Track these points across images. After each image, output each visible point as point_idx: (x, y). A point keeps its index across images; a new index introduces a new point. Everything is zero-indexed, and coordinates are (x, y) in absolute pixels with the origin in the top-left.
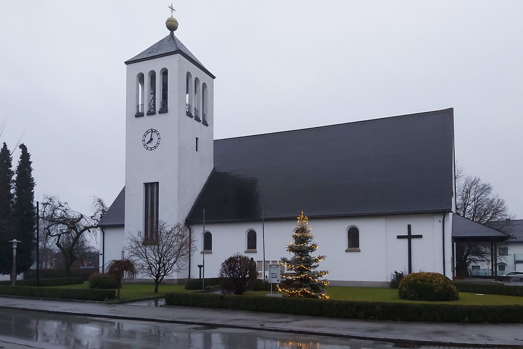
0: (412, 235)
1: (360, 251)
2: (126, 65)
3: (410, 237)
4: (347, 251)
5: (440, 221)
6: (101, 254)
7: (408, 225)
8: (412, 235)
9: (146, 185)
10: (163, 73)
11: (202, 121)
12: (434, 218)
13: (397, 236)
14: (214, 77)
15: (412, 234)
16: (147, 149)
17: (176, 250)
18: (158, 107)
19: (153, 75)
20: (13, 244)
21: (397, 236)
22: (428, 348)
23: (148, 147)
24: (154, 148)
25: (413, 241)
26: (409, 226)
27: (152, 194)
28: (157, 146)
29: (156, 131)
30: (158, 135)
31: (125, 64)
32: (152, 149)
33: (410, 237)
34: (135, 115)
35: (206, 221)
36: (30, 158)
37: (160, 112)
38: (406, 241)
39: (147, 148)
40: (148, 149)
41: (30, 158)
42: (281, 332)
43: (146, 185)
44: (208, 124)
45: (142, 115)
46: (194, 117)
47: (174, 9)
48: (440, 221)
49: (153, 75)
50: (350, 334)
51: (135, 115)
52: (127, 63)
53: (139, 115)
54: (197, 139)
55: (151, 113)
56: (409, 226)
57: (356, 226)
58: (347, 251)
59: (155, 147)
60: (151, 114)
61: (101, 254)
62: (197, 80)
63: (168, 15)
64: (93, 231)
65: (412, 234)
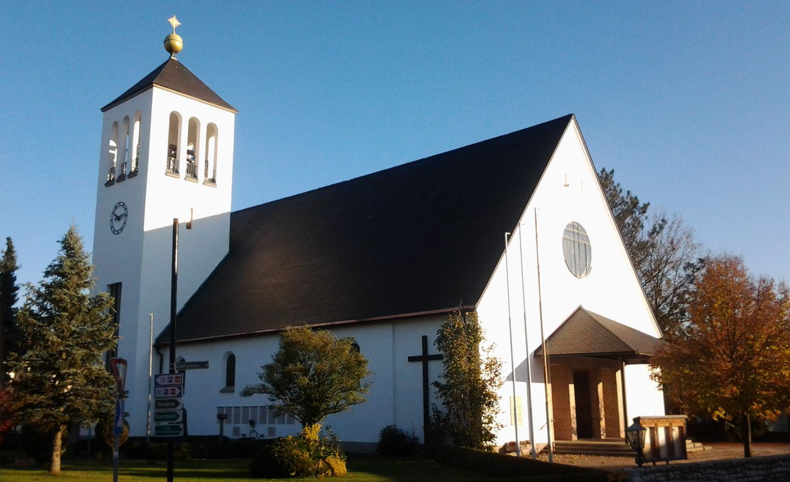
4: (222, 391)
7: (423, 337)
31: (102, 111)
38: (419, 365)
52: (104, 109)
58: (222, 391)
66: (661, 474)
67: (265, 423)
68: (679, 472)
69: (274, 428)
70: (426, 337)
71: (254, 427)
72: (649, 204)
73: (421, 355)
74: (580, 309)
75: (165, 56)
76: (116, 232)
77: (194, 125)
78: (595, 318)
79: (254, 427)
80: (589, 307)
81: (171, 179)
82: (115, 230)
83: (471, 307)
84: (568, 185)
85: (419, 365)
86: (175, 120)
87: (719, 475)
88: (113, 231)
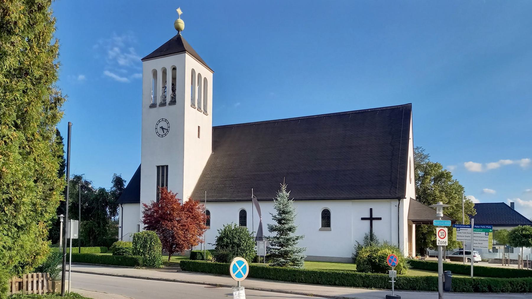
0: (373, 217)
1: (331, 231)
3: (371, 219)
4: (320, 230)
5: (396, 206)
6: (120, 227)
7: (370, 209)
8: (373, 217)
9: (158, 167)
10: (173, 69)
11: (203, 112)
12: (391, 203)
15: (373, 217)
16: (159, 136)
17: (41, 160)
18: (168, 99)
19: (164, 72)
20: (61, 219)
21: (361, 218)
22: (229, 226)
23: (160, 135)
24: (165, 135)
26: (371, 210)
27: (163, 175)
28: (167, 133)
32: (163, 136)
33: (371, 219)
37: (170, 104)
38: (368, 222)
40: (160, 136)
42: (76, 272)
43: (158, 167)
46: (197, 108)
48: (396, 206)
49: (164, 72)
55: (163, 104)
56: (371, 210)
57: (330, 209)
58: (320, 230)
60: (162, 105)
61: (120, 227)
62: (199, 75)
64: (283, 273)
65: (373, 217)
70: (372, 209)
86: (193, 71)
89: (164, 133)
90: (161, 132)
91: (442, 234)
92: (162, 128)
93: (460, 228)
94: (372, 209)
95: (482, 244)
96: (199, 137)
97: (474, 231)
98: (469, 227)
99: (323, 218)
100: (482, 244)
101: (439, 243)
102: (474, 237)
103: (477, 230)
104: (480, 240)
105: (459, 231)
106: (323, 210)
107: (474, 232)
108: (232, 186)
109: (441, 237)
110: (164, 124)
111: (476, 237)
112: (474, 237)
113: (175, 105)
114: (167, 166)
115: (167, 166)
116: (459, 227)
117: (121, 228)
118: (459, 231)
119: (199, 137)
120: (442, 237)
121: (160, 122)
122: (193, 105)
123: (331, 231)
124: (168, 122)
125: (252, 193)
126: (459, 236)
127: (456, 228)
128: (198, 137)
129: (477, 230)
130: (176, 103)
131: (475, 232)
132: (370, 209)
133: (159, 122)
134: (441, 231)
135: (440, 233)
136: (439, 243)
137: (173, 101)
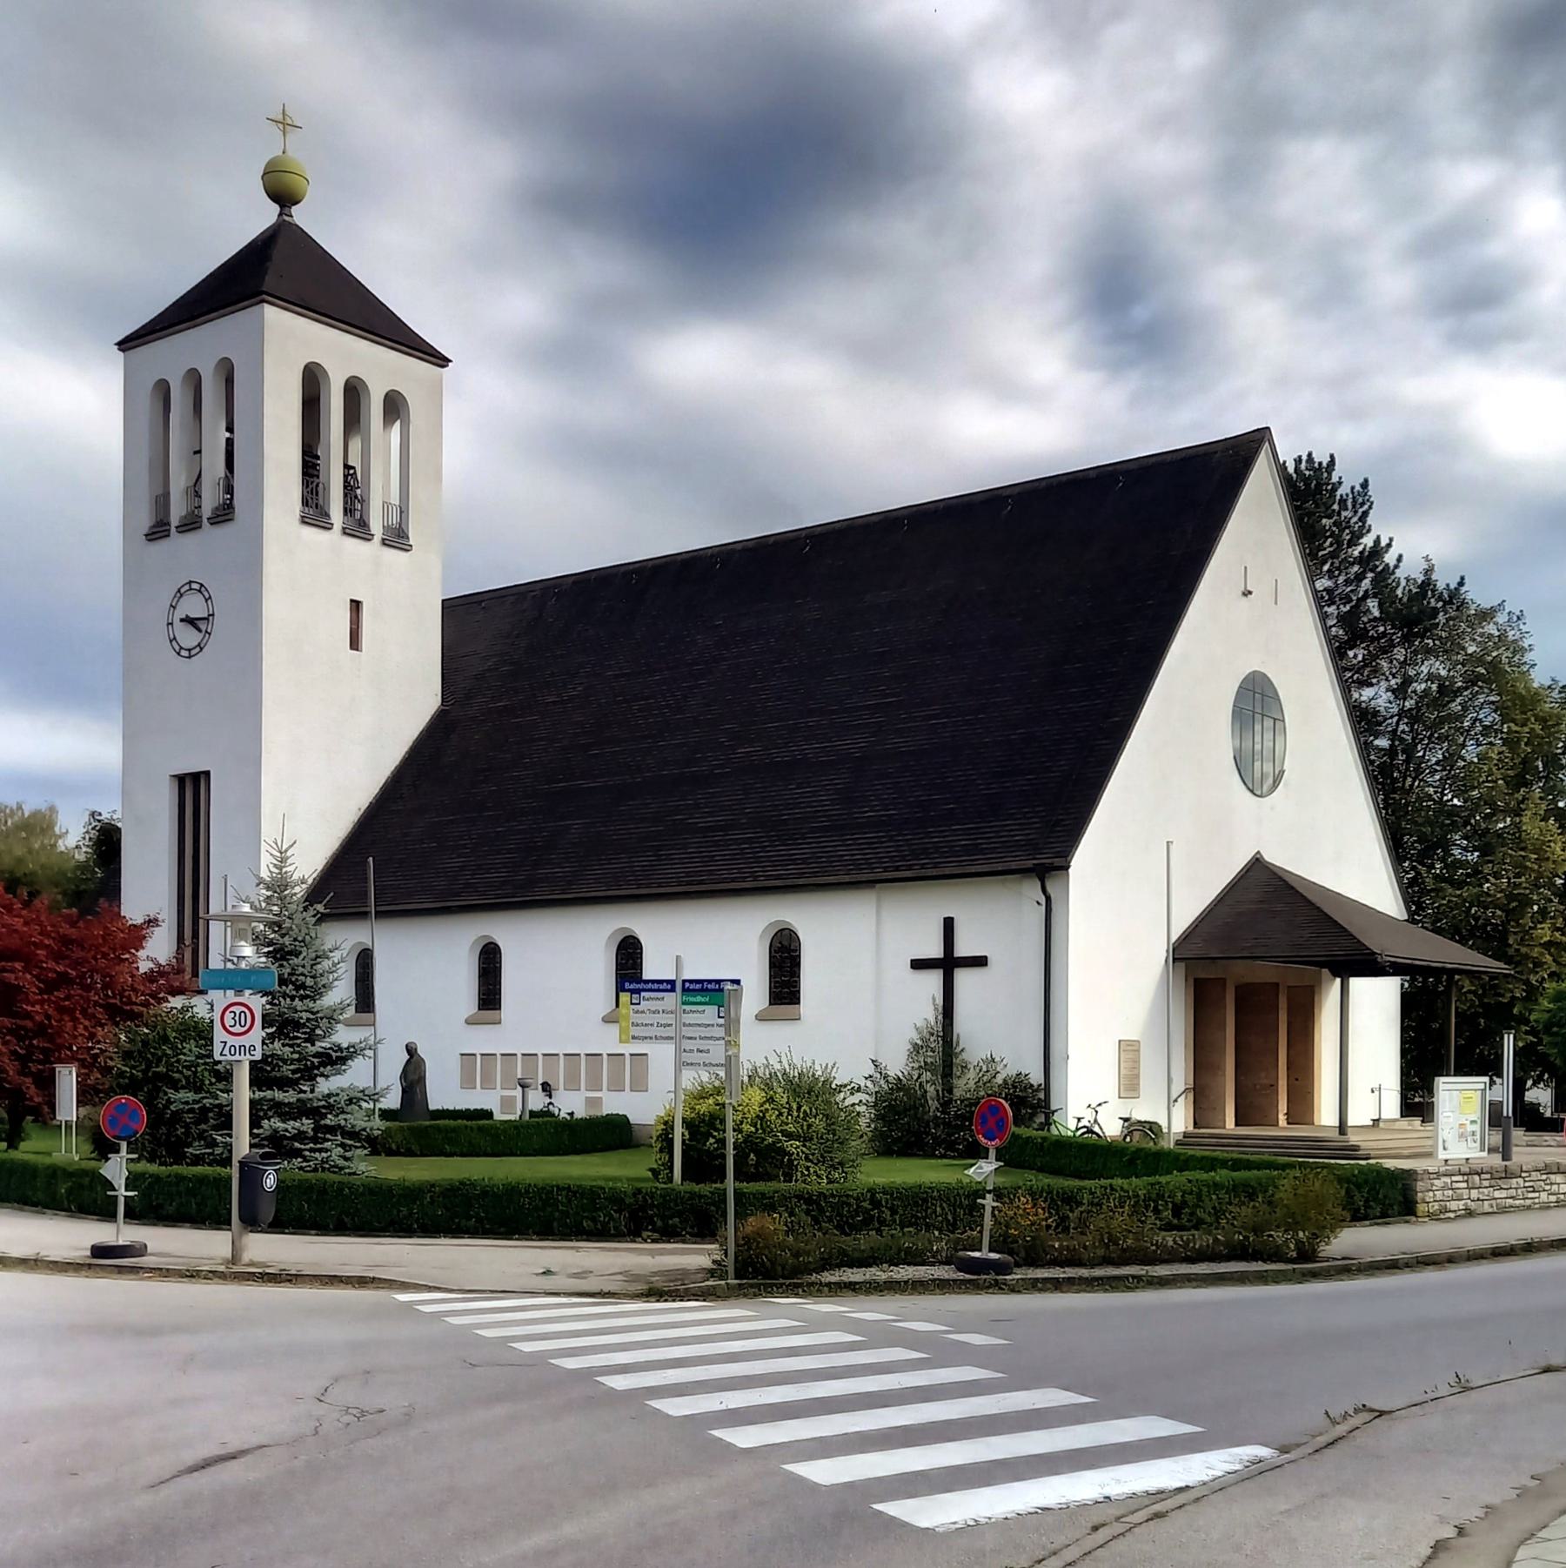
1: (500, 1023)
2: (122, 354)
3: (948, 964)
4: (469, 1022)
7: (945, 919)
9: (181, 780)
13: (912, 961)
14: (441, 361)
21: (912, 961)
25: (962, 977)
26: (949, 924)
28: (205, 641)
29: (203, 589)
30: (209, 602)
31: (119, 349)
33: (948, 964)
34: (146, 531)
35: (379, 909)
36: (1285, 462)
38: (934, 979)
39: (177, 650)
41: (1285, 462)
44: (411, 543)
45: (166, 533)
47: (295, 124)
48: (1038, 903)
50: (235, 1273)
51: (146, 535)
52: (126, 344)
53: (158, 531)
54: (356, 605)
55: (191, 524)
56: (949, 924)
58: (469, 1022)
59: (199, 645)
63: (269, 147)
66: (1460, 1178)
67: (579, 1090)
68: (1488, 1176)
69: (601, 1098)
70: (952, 919)
71: (550, 1097)
72: (1366, 481)
73: (942, 956)
74: (1257, 863)
75: (265, 215)
76: (184, 653)
77: (354, 391)
78: (1275, 870)
79: (550, 1097)
80: (1274, 857)
81: (310, 533)
82: (181, 648)
83: (1058, 862)
84: (1250, 593)
85: (934, 979)
86: (313, 379)
87: (1551, 1184)
88: (177, 648)
89: (200, 631)
90: (189, 637)
91: (237, 1018)
92: (190, 621)
93: (643, 994)
94: (952, 919)
95: (708, 1051)
96: (355, 644)
97: (684, 1003)
98: (669, 987)
99: (774, 964)
100: (708, 1051)
101: (226, 1051)
102: (684, 1025)
103: (692, 999)
104: (701, 1038)
105: (639, 1004)
106: (484, 947)
107: (684, 1007)
108: (464, 847)
109: (231, 1029)
110: (193, 606)
111: (690, 1025)
112: (684, 1025)
113: (229, 524)
114: (207, 774)
115: (207, 774)
116: (638, 991)
117: (372, 1060)
118: (639, 1004)
119: (355, 644)
120: (238, 1029)
121: (181, 595)
122: (314, 511)
123: (500, 1023)
124: (207, 596)
125: (375, 882)
126: (638, 1025)
127: (629, 994)
128: (352, 647)
129: (692, 999)
130: (233, 512)
131: (688, 1008)
132: (945, 919)
133: (178, 595)
134: (232, 1009)
135: (228, 1016)
136: (226, 1051)
137: (224, 513)
